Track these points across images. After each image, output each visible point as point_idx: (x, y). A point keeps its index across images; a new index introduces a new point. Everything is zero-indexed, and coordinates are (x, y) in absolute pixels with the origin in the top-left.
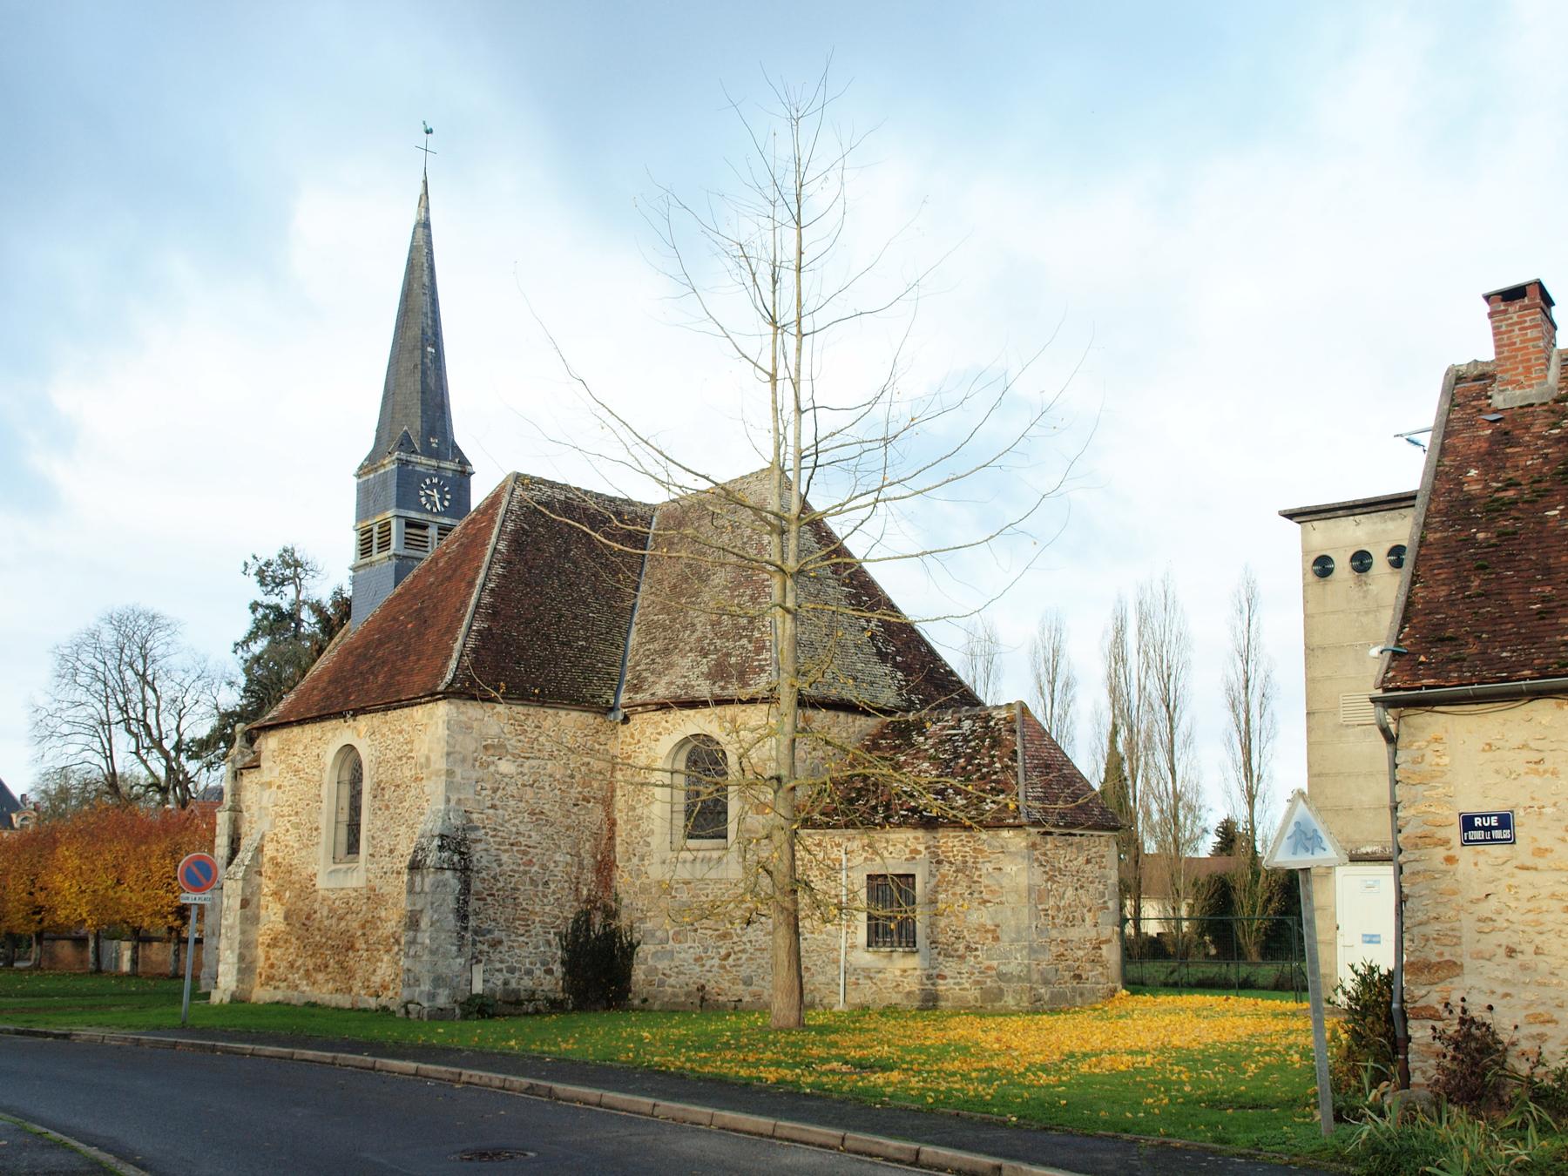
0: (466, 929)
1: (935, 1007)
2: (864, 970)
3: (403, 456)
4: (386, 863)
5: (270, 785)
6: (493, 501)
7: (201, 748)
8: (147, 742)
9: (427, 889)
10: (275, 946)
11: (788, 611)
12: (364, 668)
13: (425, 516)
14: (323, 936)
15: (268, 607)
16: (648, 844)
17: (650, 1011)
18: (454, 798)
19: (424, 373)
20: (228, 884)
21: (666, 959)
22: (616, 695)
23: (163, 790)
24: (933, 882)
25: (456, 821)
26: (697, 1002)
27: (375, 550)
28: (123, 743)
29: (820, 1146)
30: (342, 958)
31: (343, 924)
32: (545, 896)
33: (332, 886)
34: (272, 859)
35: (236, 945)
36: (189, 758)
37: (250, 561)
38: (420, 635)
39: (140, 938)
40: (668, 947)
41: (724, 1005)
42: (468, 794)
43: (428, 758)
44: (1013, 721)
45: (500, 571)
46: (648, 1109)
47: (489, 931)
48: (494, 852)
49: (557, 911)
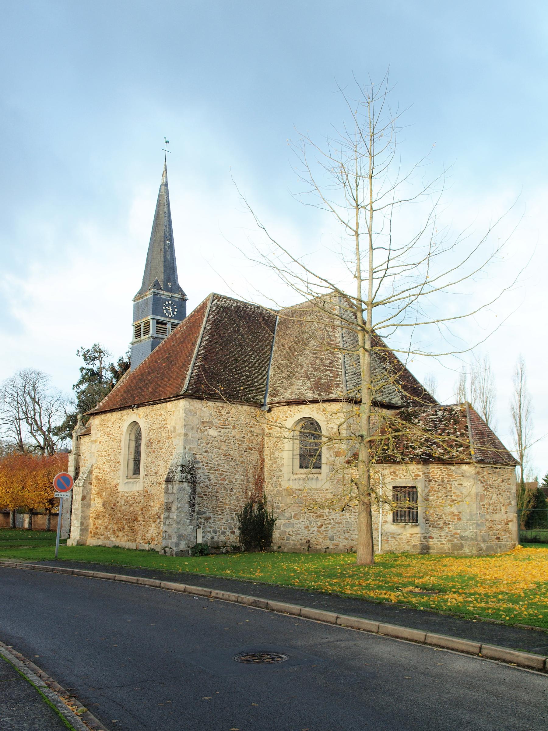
0: (194, 511)
1: (428, 553)
2: (391, 534)
3: (156, 291)
4: (153, 479)
5: (95, 441)
6: (203, 306)
7: (58, 431)
8: (35, 428)
9: (175, 491)
10: (98, 518)
11: (367, 351)
12: (141, 385)
13: (165, 319)
14: (123, 515)
15: (88, 370)
16: (281, 471)
17: (283, 552)
18: (188, 447)
19: (165, 253)
20: (75, 489)
21: (289, 528)
22: (265, 398)
23: (42, 448)
24: (427, 490)
25: (189, 459)
26: (306, 548)
27: (142, 334)
28: (25, 427)
29: (463, 652)
30: (131, 525)
31: (132, 508)
32: (231, 496)
33: (126, 490)
34: (97, 477)
35: (80, 518)
36: (54, 435)
37: (80, 350)
38: (169, 369)
39: (33, 513)
40: (291, 521)
41: (320, 550)
42: (194, 445)
43: (175, 428)
44: (465, 411)
45: (208, 338)
46: (333, 620)
47: (205, 513)
48: (207, 474)
49: (236, 503)
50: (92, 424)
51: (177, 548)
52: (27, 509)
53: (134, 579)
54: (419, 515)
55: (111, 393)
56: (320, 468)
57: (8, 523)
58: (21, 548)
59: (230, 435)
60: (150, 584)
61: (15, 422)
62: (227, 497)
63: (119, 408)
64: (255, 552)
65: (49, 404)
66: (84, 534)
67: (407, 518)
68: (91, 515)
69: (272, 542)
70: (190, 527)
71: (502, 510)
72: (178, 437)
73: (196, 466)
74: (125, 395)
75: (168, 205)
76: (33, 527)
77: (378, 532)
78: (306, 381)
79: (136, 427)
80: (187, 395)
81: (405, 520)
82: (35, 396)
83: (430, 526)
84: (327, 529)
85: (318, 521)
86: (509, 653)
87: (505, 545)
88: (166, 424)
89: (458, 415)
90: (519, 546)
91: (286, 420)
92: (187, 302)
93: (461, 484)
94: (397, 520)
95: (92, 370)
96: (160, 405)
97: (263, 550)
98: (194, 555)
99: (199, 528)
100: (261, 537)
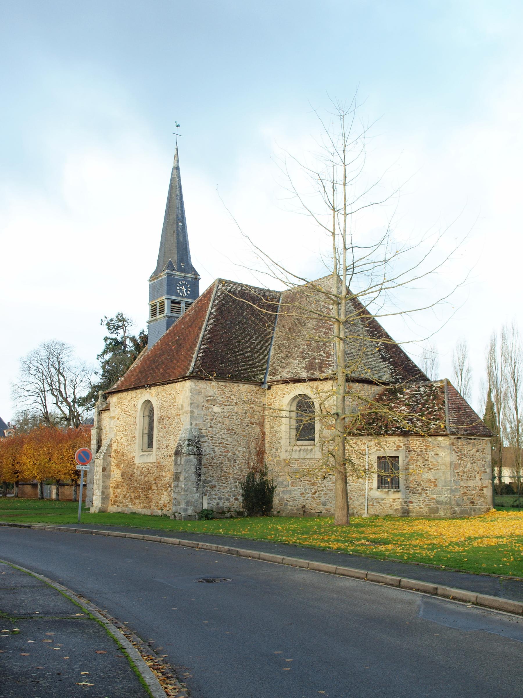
0: (200, 480)
1: (408, 516)
2: (376, 499)
3: (169, 272)
4: (165, 451)
5: (114, 418)
6: (209, 291)
8: (61, 399)
9: (182, 463)
10: (117, 488)
11: (341, 339)
12: (154, 366)
13: (179, 298)
14: (138, 484)
15: (112, 339)
16: (279, 443)
19: (178, 234)
21: (288, 493)
22: (265, 377)
24: (407, 460)
25: (195, 433)
26: (302, 513)
27: (158, 314)
28: (50, 399)
31: (146, 478)
32: (234, 466)
33: (141, 462)
34: (116, 450)
35: (101, 487)
36: (79, 406)
37: (104, 319)
38: (178, 351)
40: (289, 489)
41: (314, 514)
43: (182, 406)
44: (443, 387)
45: (213, 322)
47: (210, 482)
48: (212, 447)
49: (239, 473)
50: (111, 401)
51: (185, 513)
52: (54, 481)
53: (141, 536)
54: (400, 482)
55: (133, 365)
56: (314, 440)
57: (36, 494)
58: (49, 515)
59: (233, 411)
60: (153, 539)
61: (41, 394)
62: (231, 468)
63: (134, 388)
64: (257, 516)
65: (73, 375)
66: (105, 503)
67: (390, 485)
68: (111, 485)
69: (272, 508)
70: (197, 494)
71: (477, 477)
72: (185, 414)
73: (202, 440)
74: (139, 375)
75: (180, 187)
76: (60, 497)
77: (365, 498)
78: (302, 360)
79: (149, 404)
80: (193, 377)
81: (389, 487)
82: (59, 368)
83: (410, 492)
84: (320, 495)
85: (312, 489)
86: (382, 577)
87: (479, 508)
88: (175, 402)
89: (437, 391)
90: (494, 510)
91: (283, 397)
92: (200, 281)
93: (437, 454)
94: (382, 487)
95: (115, 340)
96: (169, 385)
97: (264, 514)
98: (200, 519)
99: (206, 495)
100: (263, 503)
